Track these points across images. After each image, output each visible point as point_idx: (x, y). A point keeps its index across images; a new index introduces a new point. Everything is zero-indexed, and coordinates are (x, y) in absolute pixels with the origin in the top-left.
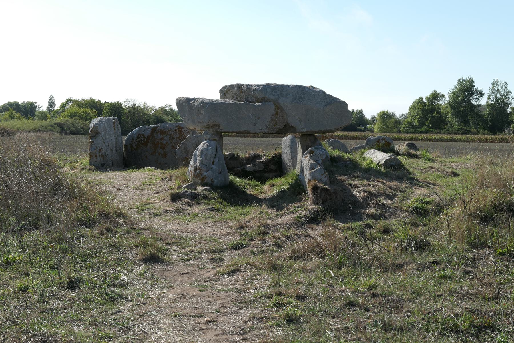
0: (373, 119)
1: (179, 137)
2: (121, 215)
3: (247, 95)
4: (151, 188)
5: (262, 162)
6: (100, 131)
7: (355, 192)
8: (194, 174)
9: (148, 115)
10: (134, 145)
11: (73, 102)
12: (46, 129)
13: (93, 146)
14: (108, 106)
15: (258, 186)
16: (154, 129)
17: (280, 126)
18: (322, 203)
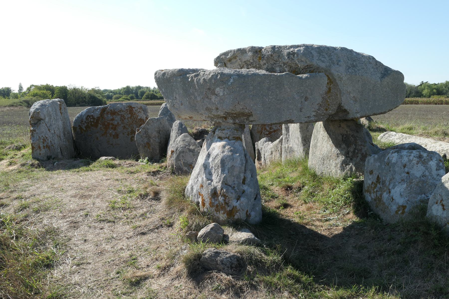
1: (131, 117)
6: (42, 117)
9: (84, 94)
10: (83, 127)
13: (35, 135)
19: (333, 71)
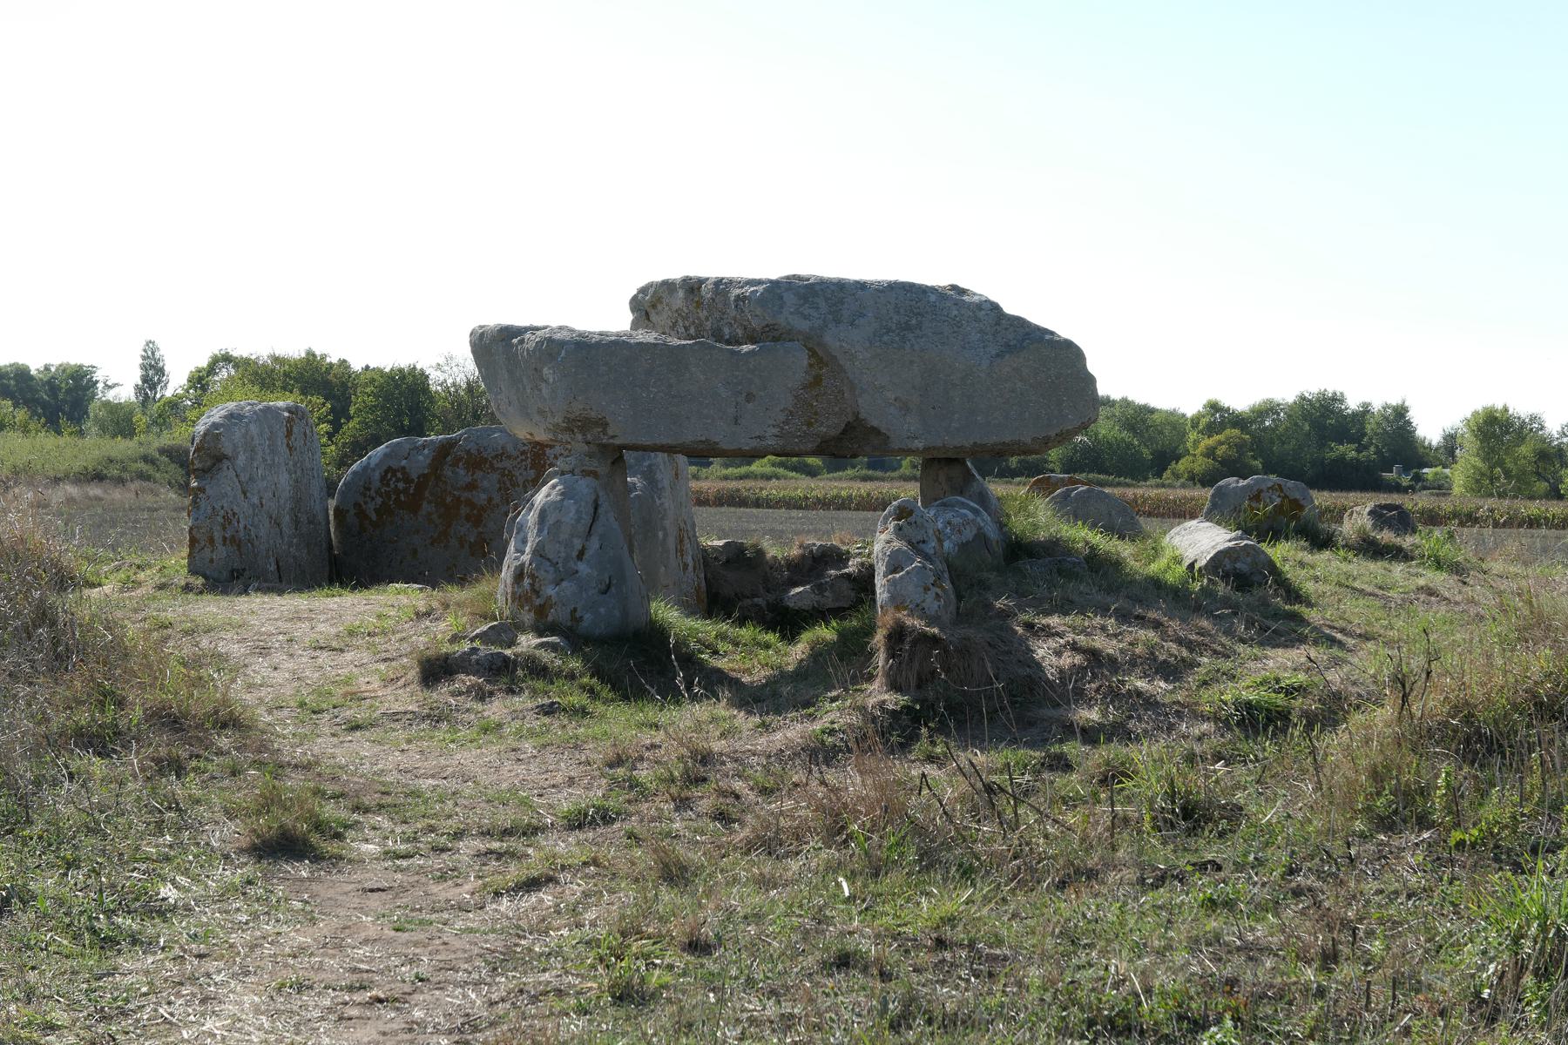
0: (1451, 443)
2: (229, 722)
3: (717, 315)
4: (370, 646)
5: (849, 575)
6: (228, 451)
7: (1042, 650)
8: (513, 593)
10: (370, 509)
11: (236, 366)
12: (124, 469)
13: (203, 504)
14: (373, 380)
15: (767, 646)
16: (445, 450)
17: (829, 426)
18: (919, 687)
19: (828, 338)
